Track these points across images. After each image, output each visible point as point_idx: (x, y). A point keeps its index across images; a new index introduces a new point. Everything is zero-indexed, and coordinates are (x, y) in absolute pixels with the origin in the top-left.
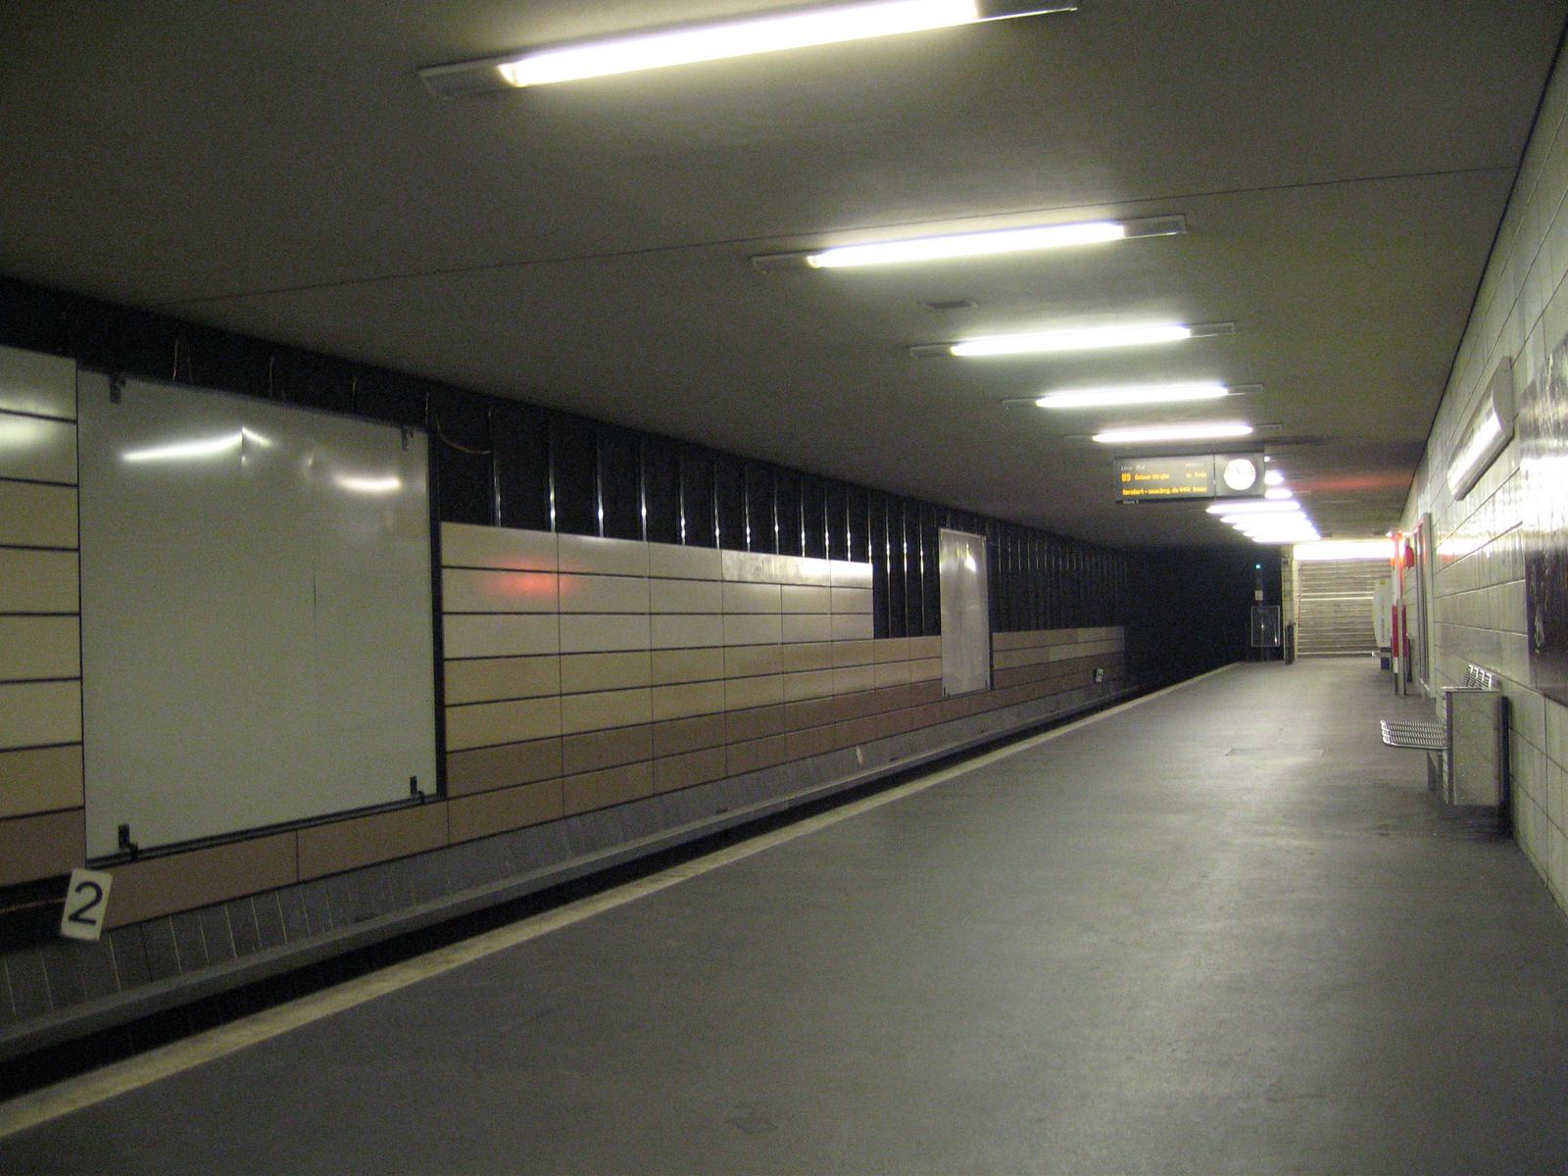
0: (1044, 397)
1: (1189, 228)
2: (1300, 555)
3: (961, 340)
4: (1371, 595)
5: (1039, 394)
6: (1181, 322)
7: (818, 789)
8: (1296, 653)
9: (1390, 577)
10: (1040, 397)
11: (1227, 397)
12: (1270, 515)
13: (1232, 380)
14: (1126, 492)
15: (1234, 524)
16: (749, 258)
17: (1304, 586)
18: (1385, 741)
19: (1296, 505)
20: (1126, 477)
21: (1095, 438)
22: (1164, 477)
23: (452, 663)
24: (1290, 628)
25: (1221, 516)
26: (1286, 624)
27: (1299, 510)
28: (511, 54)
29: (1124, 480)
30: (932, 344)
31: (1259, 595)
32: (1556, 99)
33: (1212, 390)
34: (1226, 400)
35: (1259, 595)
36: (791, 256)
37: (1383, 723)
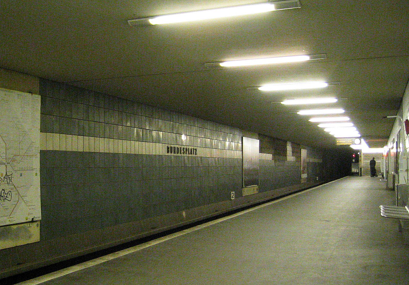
0: (283, 101)
1: (328, 57)
2: (363, 152)
3: (224, 60)
4: (380, 161)
5: (259, 86)
6: (325, 82)
7: (163, 241)
8: (362, 174)
9: (394, 204)
10: (298, 112)
11: (309, 60)
12: (363, 147)
13: (338, 97)
14: (337, 144)
15: (334, 135)
16: (127, 20)
17: (364, 158)
18: (382, 215)
19: (352, 124)
20: (338, 142)
21: (282, 103)
22: (344, 142)
23: (408, 168)
24: (361, 168)
25: (324, 128)
26: (360, 167)
27: (354, 126)
28: (152, 17)
29: (337, 142)
30: (139, 18)
31: (354, 160)
32: (407, 87)
33: (333, 100)
34: (308, 62)
35: (354, 160)
36: (142, 19)
37: (381, 207)
